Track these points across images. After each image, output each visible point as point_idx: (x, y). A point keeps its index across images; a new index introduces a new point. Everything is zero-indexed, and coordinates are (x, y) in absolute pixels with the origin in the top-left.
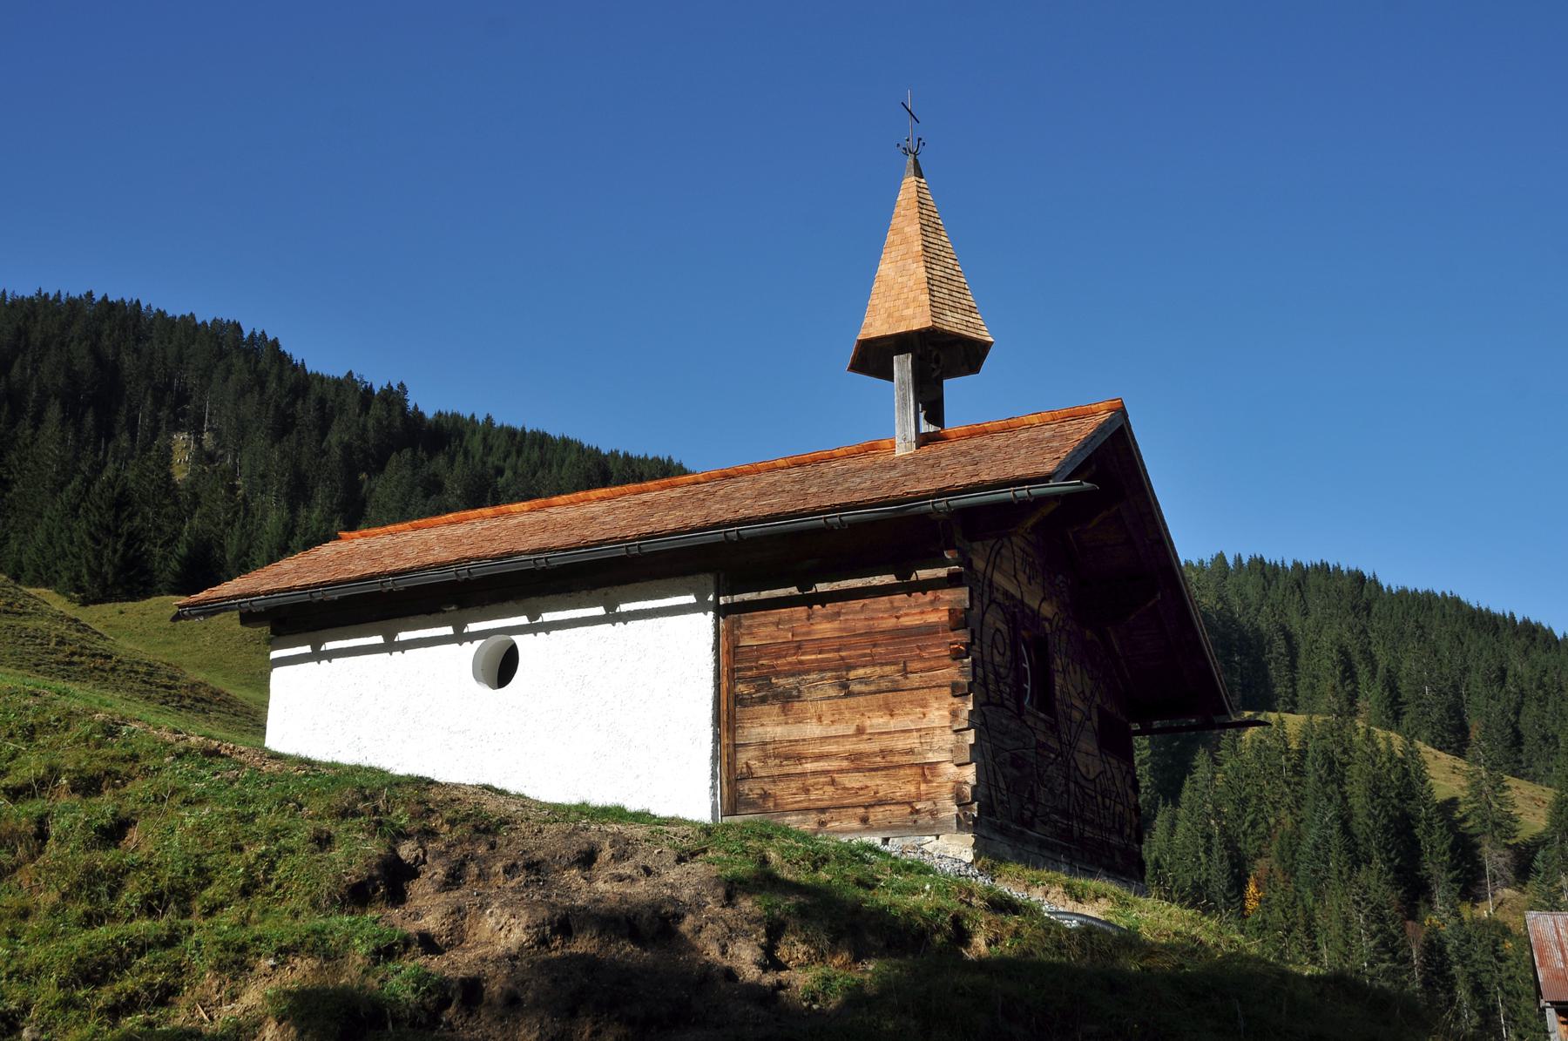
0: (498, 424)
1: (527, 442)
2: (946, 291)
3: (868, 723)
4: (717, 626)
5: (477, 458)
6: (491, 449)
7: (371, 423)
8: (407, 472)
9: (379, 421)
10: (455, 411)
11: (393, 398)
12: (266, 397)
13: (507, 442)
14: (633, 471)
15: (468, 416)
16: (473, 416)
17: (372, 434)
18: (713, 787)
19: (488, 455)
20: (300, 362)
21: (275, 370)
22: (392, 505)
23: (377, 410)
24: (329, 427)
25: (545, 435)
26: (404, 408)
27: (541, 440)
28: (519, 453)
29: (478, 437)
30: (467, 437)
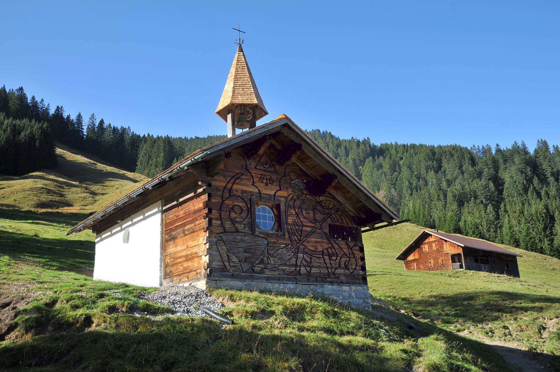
0: (399, 144)
1: (409, 148)
2: (241, 89)
3: (188, 244)
4: (162, 217)
5: (394, 156)
6: (398, 152)
7: (360, 151)
8: (371, 164)
9: (363, 150)
10: (386, 143)
11: (366, 142)
12: (329, 149)
13: (403, 149)
14: (443, 151)
15: (390, 143)
16: (391, 143)
17: (361, 154)
18: (160, 270)
19: (397, 154)
20: (338, 137)
21: (331, 141)
22: (368, 174)
23: (362, 147)
24: (348, 155)
25: (414, 145)
26: (370, 145)
27: (413, 146)
28: (407, 151)
29: (394, 149)
30: (390, 150)
